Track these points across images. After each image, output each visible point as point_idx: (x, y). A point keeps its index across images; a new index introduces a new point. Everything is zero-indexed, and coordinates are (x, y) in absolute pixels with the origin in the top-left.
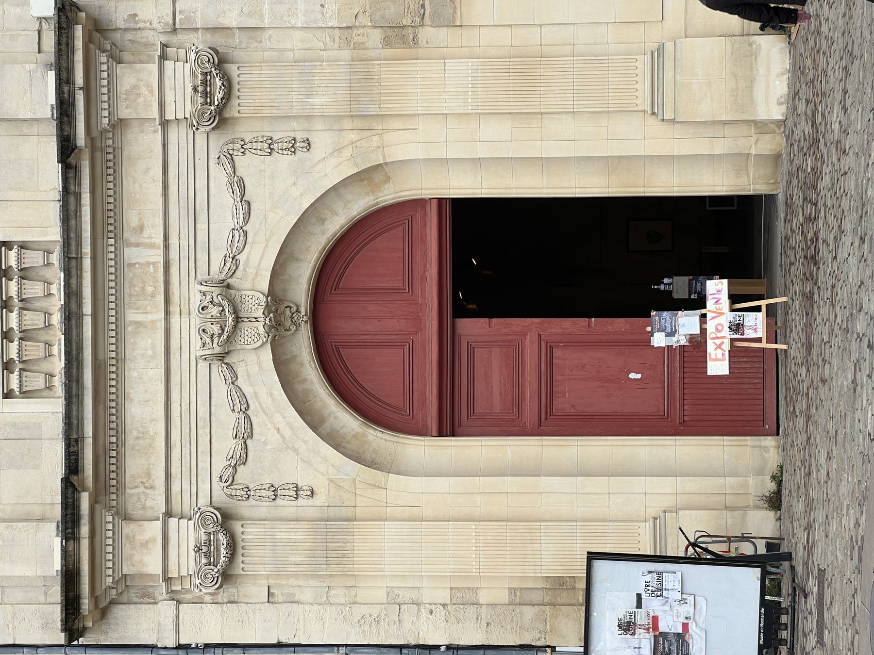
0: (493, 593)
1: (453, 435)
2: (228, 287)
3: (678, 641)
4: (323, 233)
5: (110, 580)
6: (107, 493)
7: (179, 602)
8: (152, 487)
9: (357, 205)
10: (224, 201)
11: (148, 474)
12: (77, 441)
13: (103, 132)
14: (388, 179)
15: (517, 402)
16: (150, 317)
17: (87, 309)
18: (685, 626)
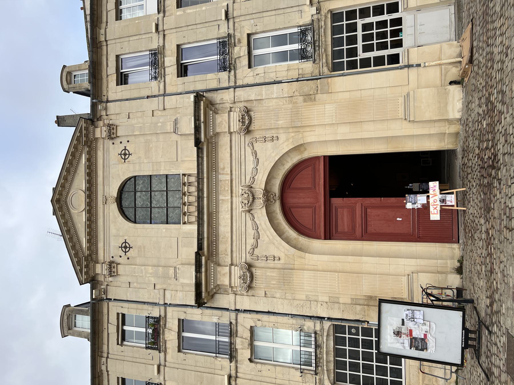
0: (345, 299)
1: (330, 239)
2: (251, 187)
3: (422, 342)
4: (284, 169)
5: (212, 286)
6: (212, 256)
7: (236, 294)
8: (227, 255)
9: (295, 159)
10: (250, 158)
11: (226, 251)
12: (201, 239)
13: (211, 137)
14: (306, 149)
15: (354, 228)
16: (227, 198)
17: (205, 195)
18: (425, 335)
